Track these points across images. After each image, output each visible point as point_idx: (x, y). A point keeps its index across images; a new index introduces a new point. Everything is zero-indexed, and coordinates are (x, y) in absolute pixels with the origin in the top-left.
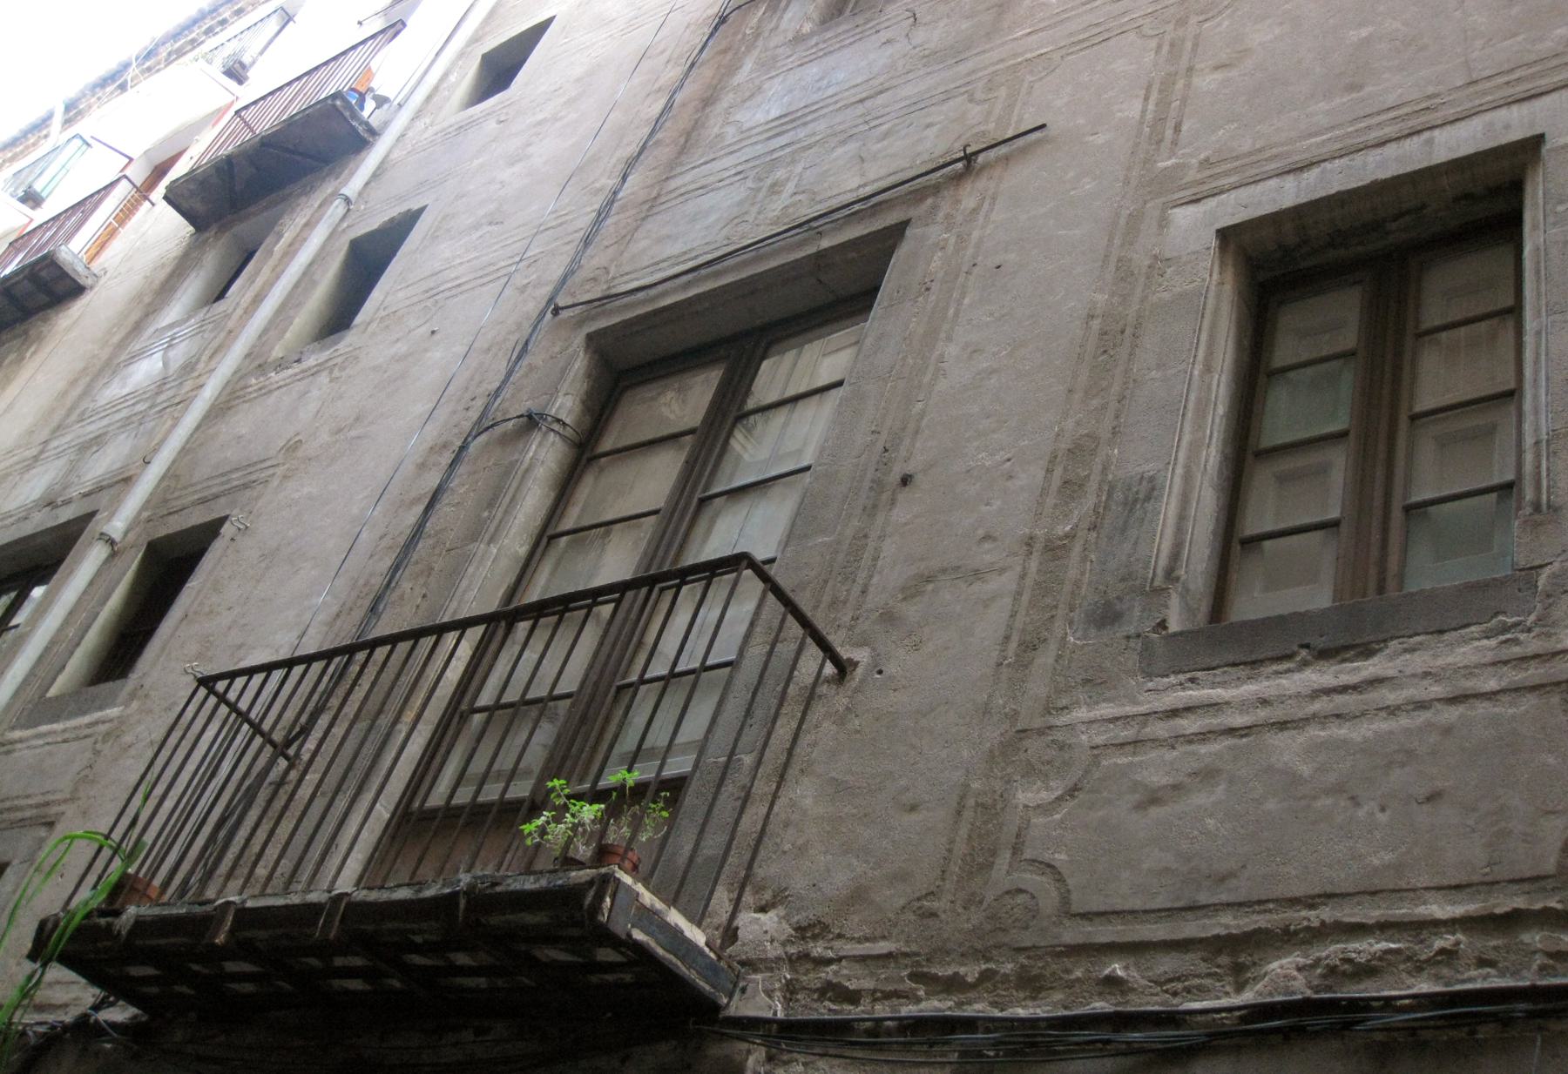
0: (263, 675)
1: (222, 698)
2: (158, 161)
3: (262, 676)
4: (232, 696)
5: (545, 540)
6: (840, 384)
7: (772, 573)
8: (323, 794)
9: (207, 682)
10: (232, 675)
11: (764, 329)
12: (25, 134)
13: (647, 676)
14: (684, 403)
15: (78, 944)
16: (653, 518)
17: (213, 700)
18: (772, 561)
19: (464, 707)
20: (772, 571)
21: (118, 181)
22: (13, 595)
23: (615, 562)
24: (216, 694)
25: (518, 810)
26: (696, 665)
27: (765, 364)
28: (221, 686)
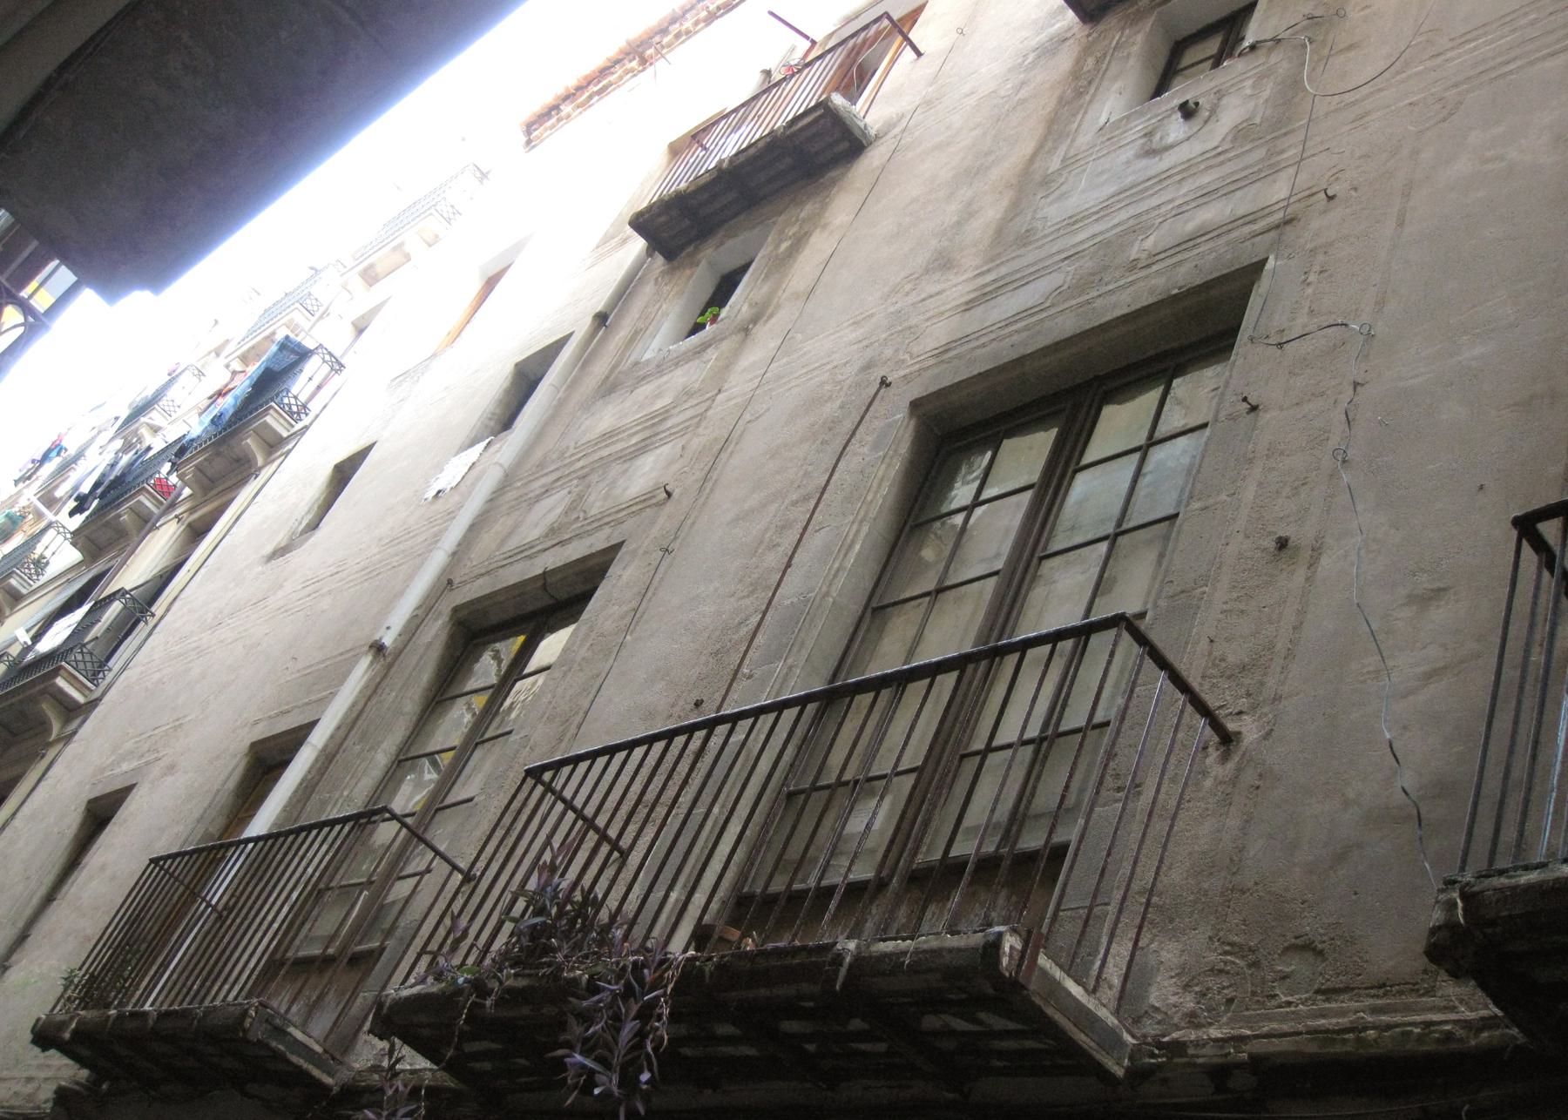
0: (588, 762)
1: (549, 788)
2: (491, 273)
3: (772, 717)
4: (558, 784)
5: (1035, 561)
6: (1205, 426)
7: (1142, 628)
8: (1173, 780)
9: (535, 773)
10: (557, 766)
11: (1100, 379)
12: (589, 81)
13: (995, 743)
14: (1026, 456)
15: (44, 1037)
16: (993, 580)
17: (540, 789)
18: (1142, 615)
19: (322, 886)
20: (1143, 625)
21: (807, 37)
22: (521, 639)
23: (952, 632)
24: (543, 784)
25: (998, 866)
26: (1082, 722)
27: (1109, 411)
28: (547, 776)
